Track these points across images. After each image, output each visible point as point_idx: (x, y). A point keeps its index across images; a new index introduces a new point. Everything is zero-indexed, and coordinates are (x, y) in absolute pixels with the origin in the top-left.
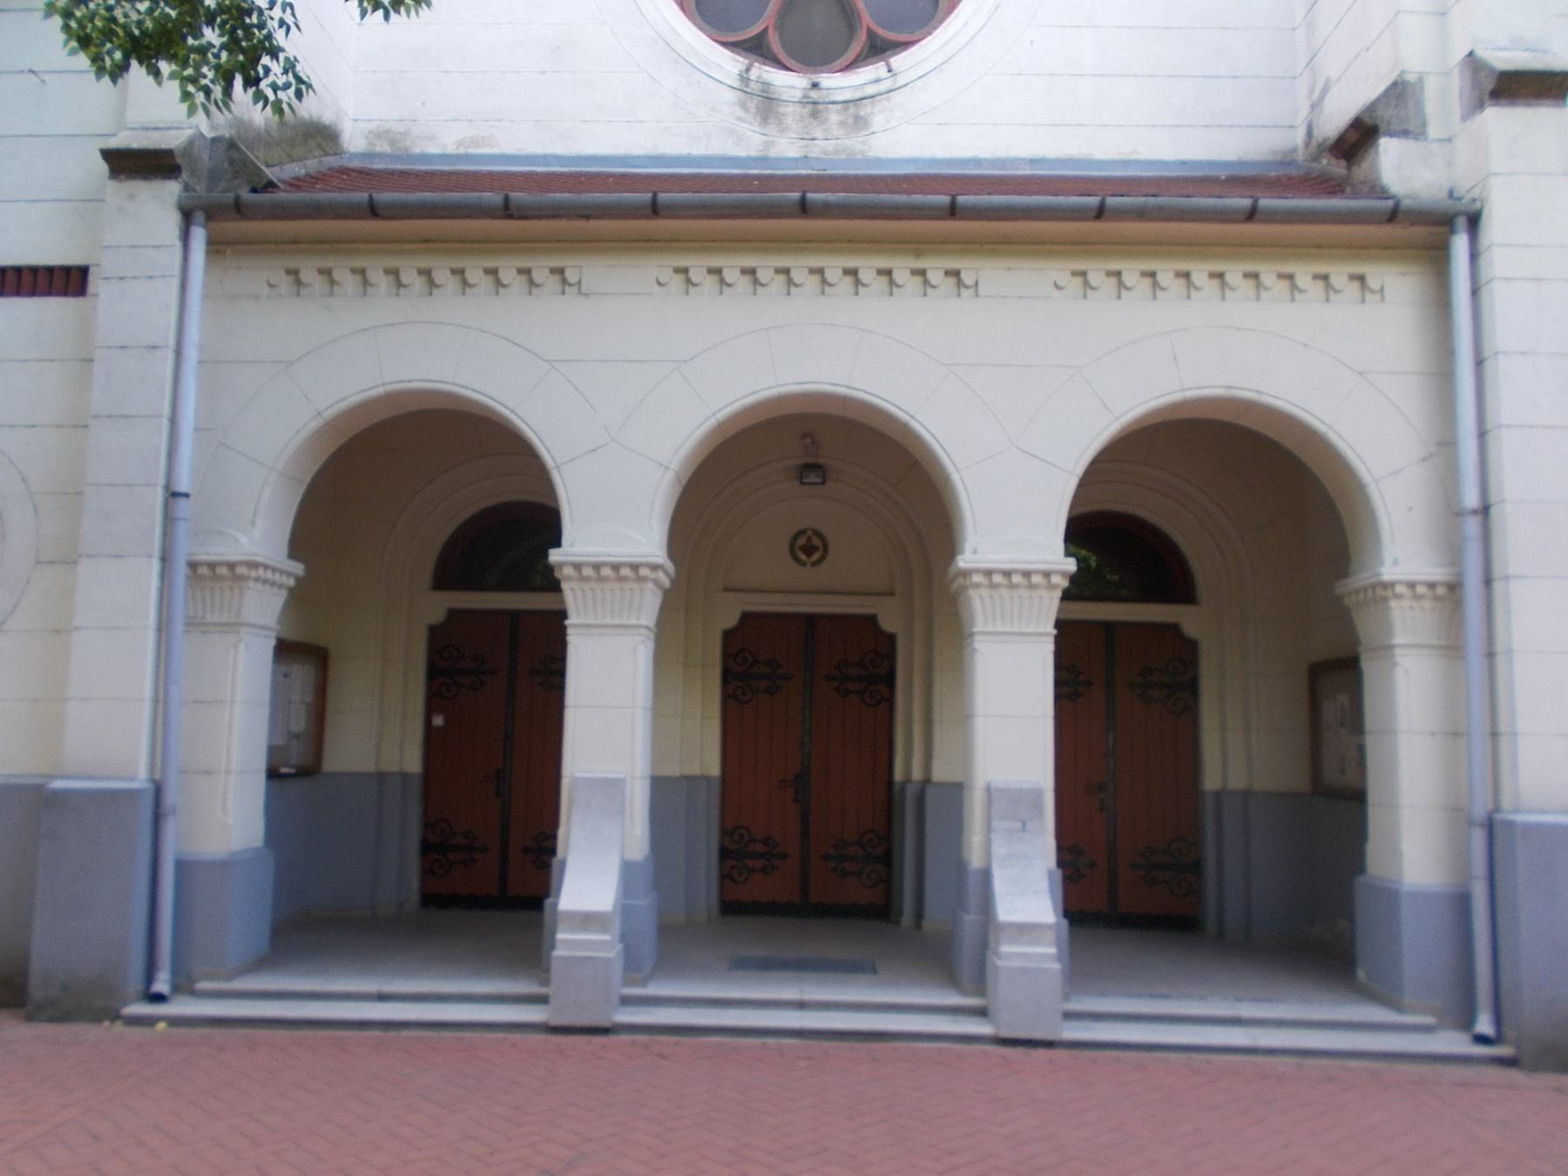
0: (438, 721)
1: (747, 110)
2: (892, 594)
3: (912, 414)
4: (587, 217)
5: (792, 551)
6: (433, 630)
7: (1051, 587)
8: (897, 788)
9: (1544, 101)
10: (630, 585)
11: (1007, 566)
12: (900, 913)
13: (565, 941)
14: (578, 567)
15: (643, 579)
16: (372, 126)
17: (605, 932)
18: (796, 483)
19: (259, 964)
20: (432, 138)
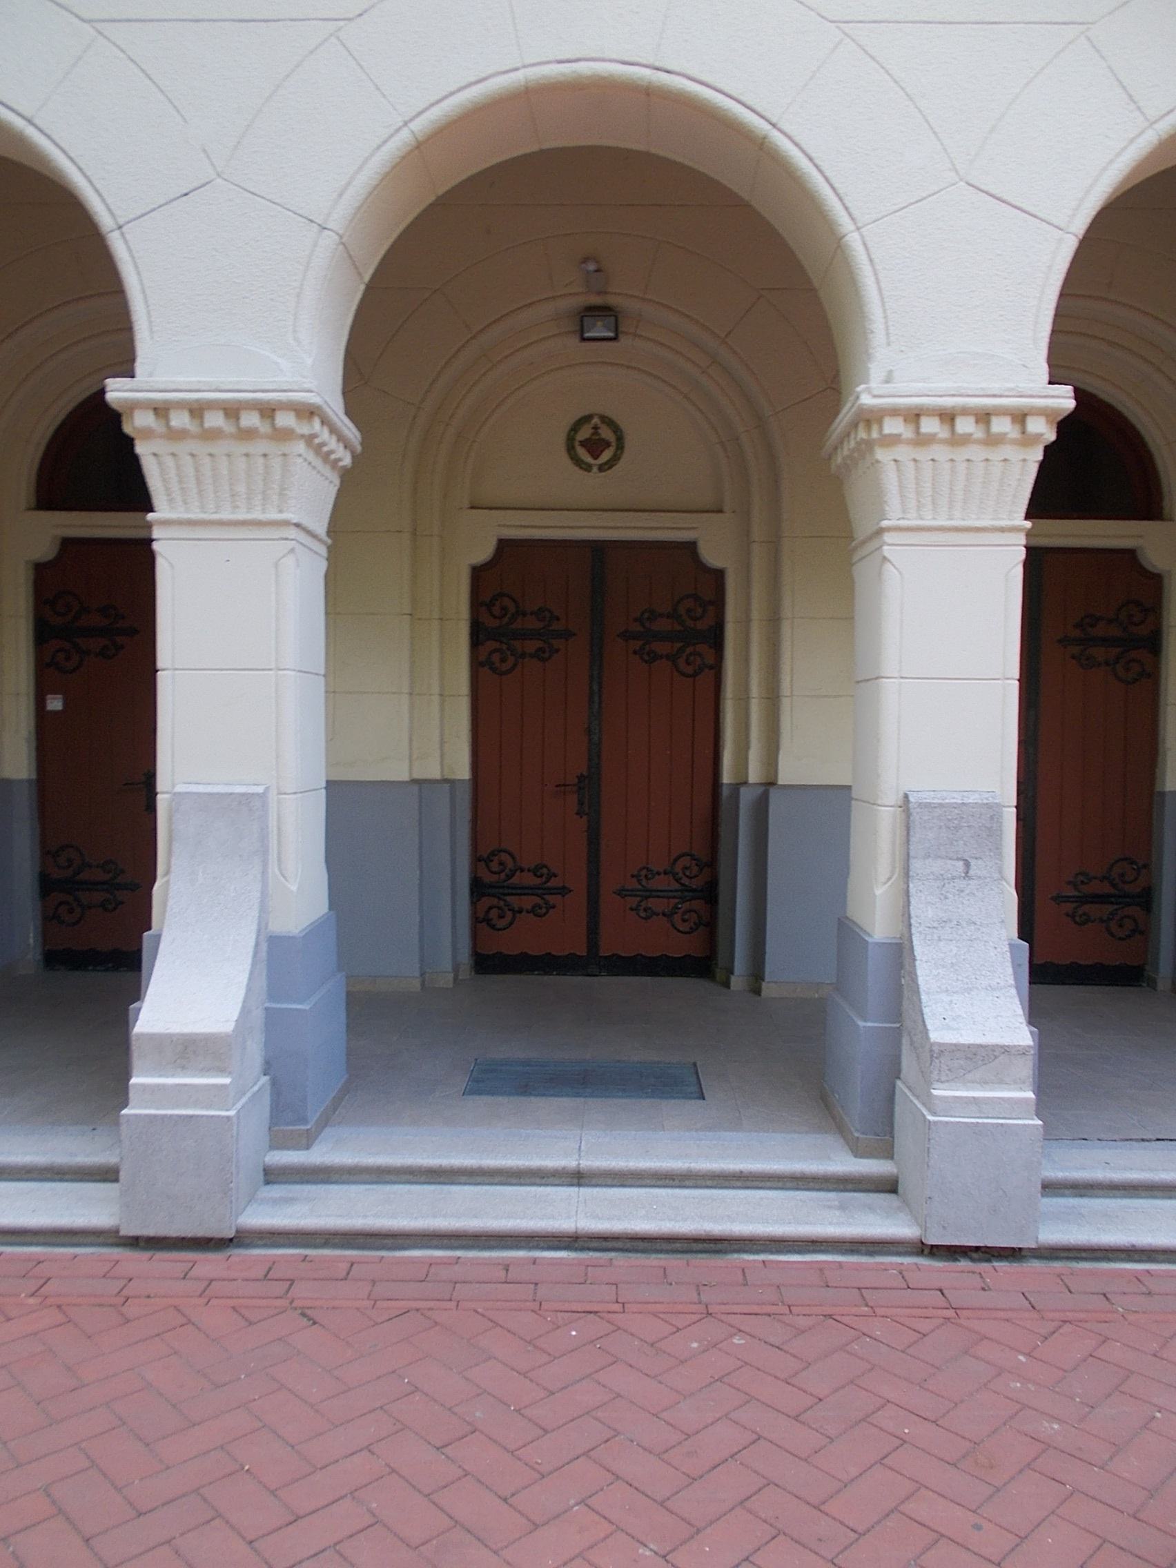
0: (55, 704)
2: (720, 511)
3: (774, 120)
5: (570, 449)
6: (40, 570)
7: (1027, 440)
8: (725, 792)
10: (259, 447)
11: (948, 402)
12: (730, 971)
13: (145, 1087)
14: (161, 410)
15: (284, 435)
17: (222, 1071)
18: (574, 341)
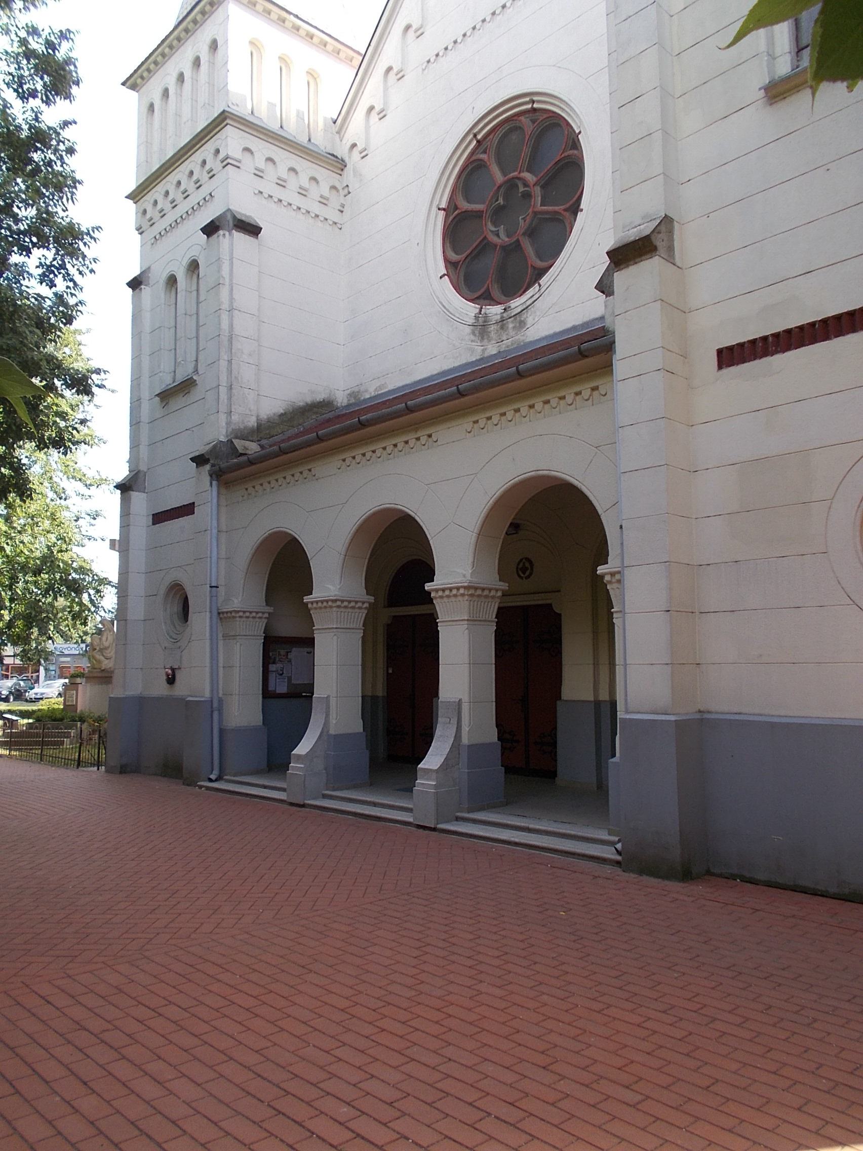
1: (475, 335)
4: (310, 446)
9: (643, 258)
16: (348, 392)
19: (257, 772)
20: (366, 391)
